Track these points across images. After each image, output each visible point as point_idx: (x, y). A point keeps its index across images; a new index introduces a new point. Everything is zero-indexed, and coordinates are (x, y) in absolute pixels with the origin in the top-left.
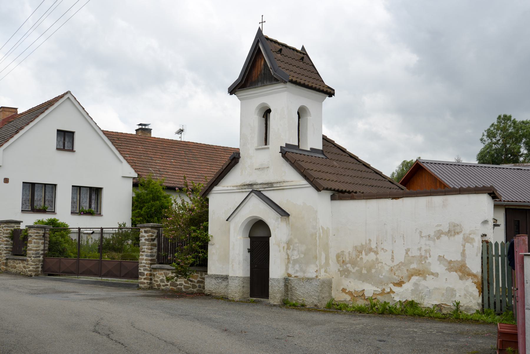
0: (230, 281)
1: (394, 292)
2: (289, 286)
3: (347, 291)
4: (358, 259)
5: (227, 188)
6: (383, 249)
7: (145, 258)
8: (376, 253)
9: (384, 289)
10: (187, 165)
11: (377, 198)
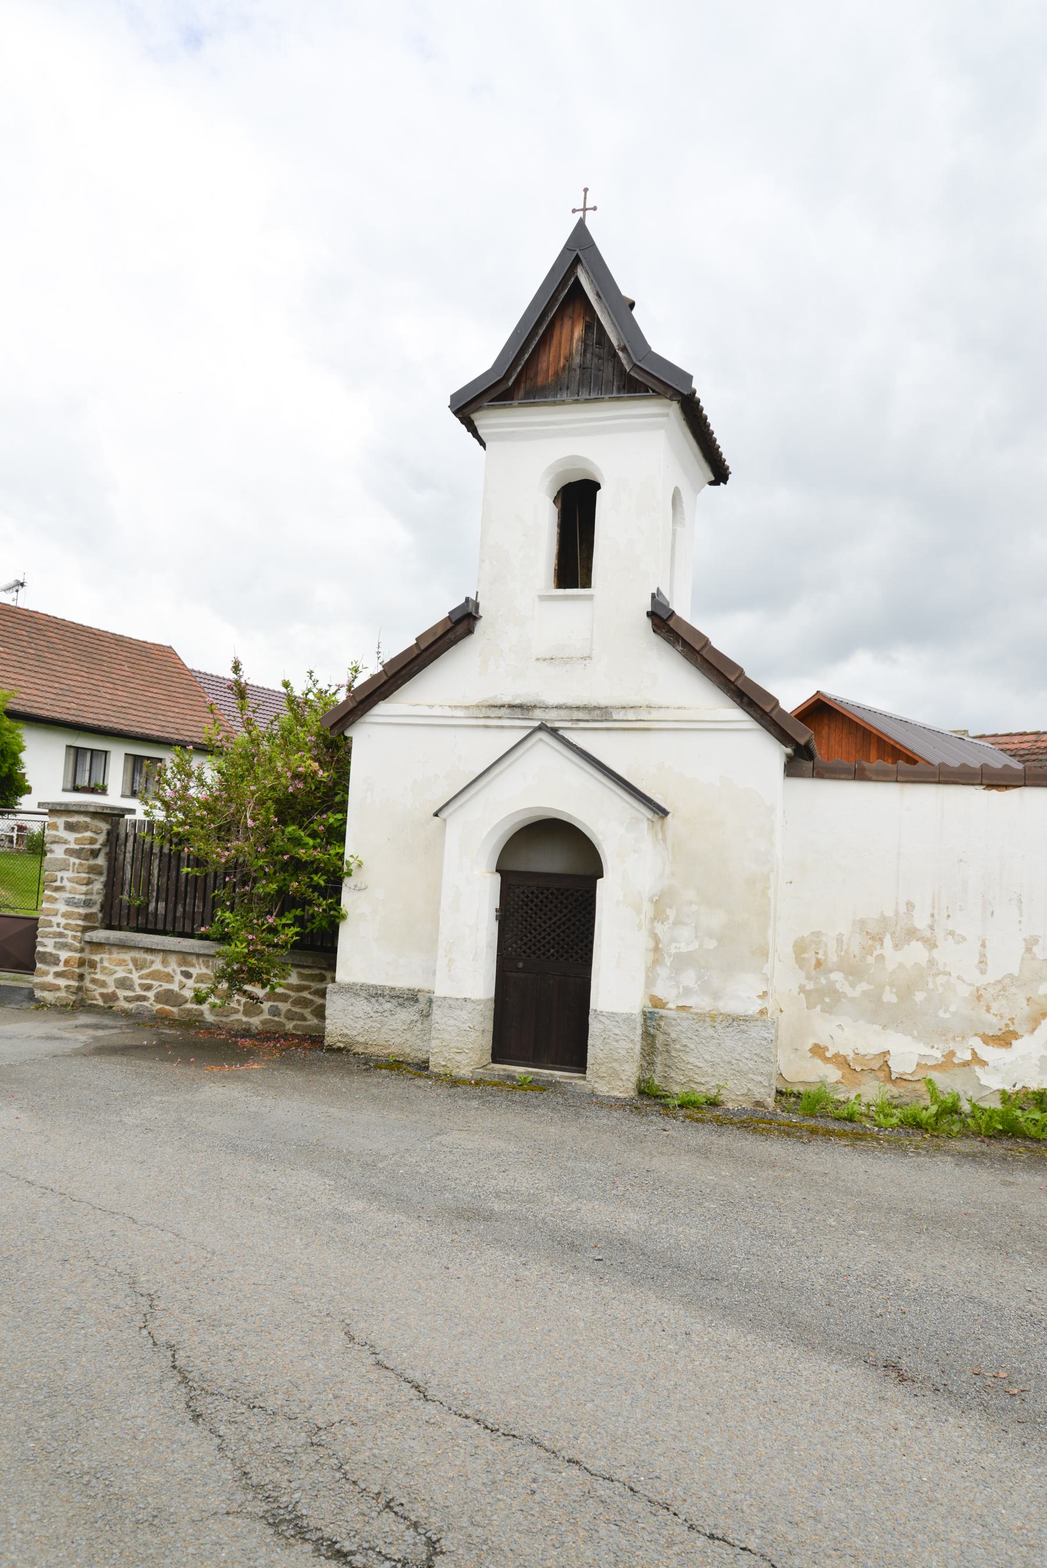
0: (437, 1014)
1: (983, 1063)
2: (660, 1038)
3: (828, 1054)
4: (870, 960)
5: (427, 712)
6: (951, 933)
7: (63, 908)
8: (931, 944)
9: (952, 1054)
10: (36, 663)
11: (939, 782)
